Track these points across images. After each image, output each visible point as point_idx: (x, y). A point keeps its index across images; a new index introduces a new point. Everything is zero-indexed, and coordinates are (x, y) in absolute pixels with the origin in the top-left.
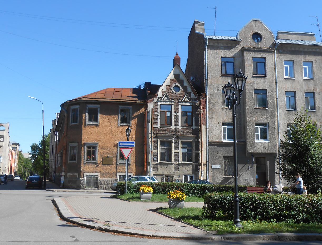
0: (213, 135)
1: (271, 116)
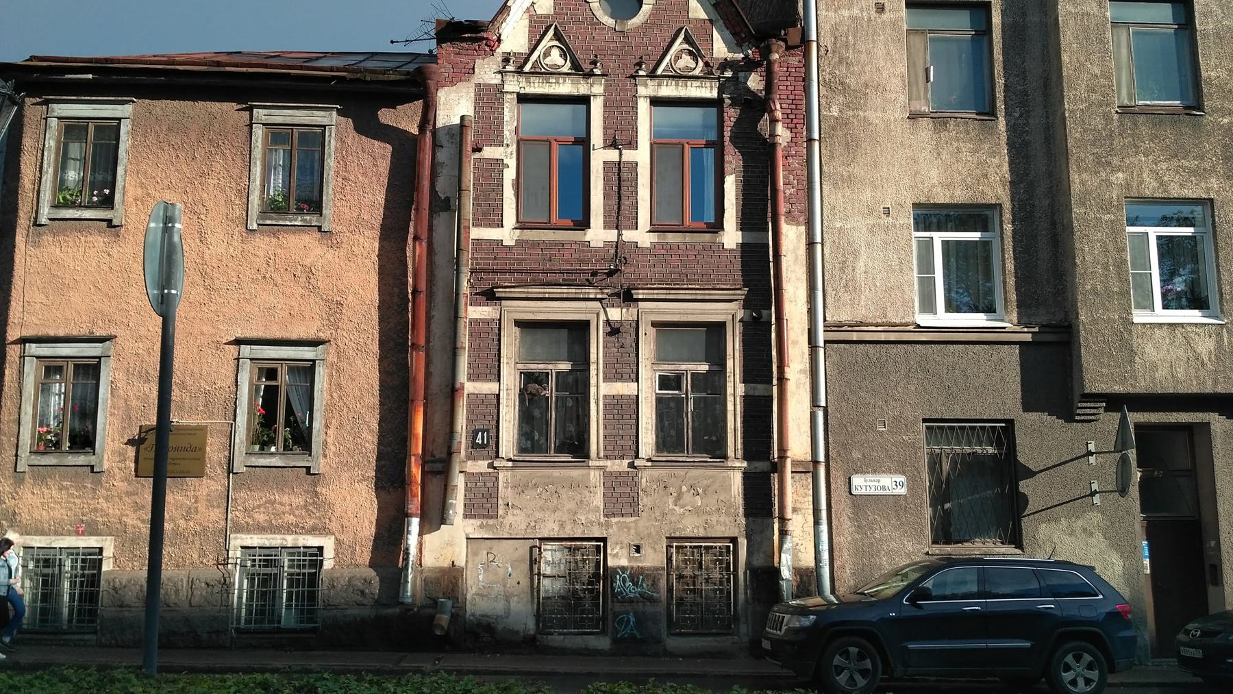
0: (851, 287)
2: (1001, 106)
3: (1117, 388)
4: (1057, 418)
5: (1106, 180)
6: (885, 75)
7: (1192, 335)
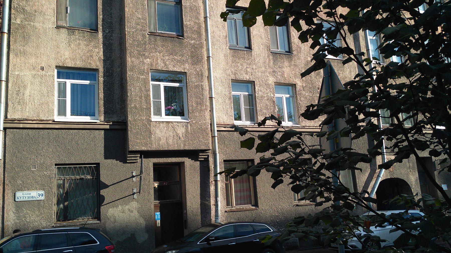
0: (22, 102)
1: (192, 57)
2: (100, 27)
3: (143, 148)
4: (120, 162)
5: (142, 61)
6: (45, 7)
7: (176, 126)
